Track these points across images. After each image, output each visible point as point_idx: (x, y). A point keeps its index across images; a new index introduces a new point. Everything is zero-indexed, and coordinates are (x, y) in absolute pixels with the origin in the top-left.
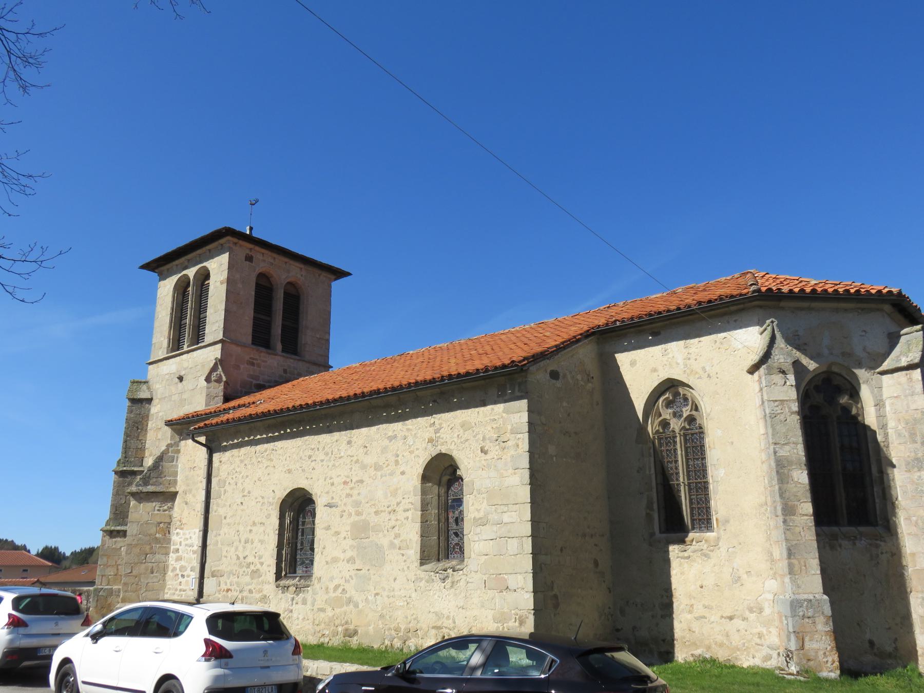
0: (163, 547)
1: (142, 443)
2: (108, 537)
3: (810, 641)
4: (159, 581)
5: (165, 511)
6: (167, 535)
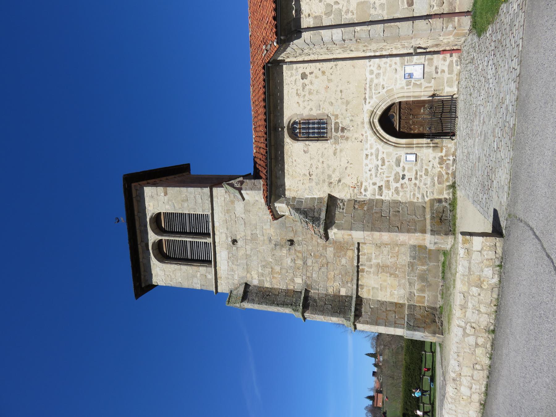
0: (376, 204)
1: (282, 292)
2: (360, 318)
3: (421, 290)
4: (407, 206)
5: (344, 205)
6: (366, 202)
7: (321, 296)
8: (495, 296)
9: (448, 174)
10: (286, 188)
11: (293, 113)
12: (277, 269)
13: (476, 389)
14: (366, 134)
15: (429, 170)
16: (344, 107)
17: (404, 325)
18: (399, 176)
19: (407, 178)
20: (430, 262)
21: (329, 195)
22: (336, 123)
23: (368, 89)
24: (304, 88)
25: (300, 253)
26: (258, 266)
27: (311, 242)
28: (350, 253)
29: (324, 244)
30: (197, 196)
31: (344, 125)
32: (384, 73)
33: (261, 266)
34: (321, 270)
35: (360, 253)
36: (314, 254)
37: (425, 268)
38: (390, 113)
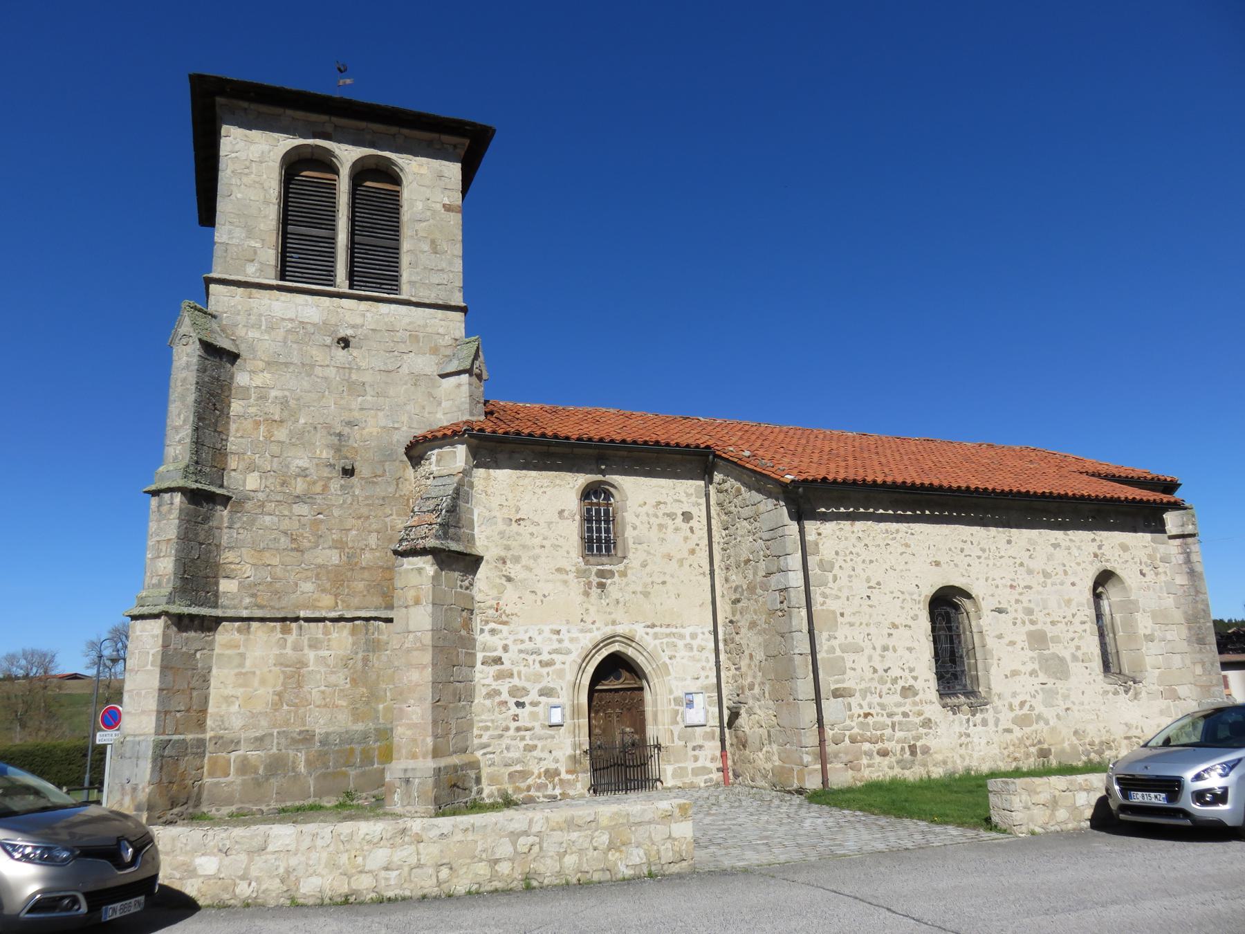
2: (175, 629)
7: (217, 532)
8: (596, 877)
9: (529, 788)
10: (491, 471)
11: (629, 494)
12: (281, 434)
13: (387, 879)
14: (595, 629)
15: (535, 753)
16: (639, 589)
17: (164, 733)
18: (522, 696)
19: (519, 711)
20: (317, 779)
21: (482, 558)
22: (612, 574)
23: (668, 631)
24: (668, 515)
25: (323, 490)
26: (285, 390)
27: (350, 514)
28: (327, 600)
29: (347, 543)
30: (445, 276)
31: (610, 589)
32: (693, 658)
33: (286, 396)
34: (282, 535)
35: (327, 623)
36: (322, 521)
37: (302, 768)
38: (625, 674)
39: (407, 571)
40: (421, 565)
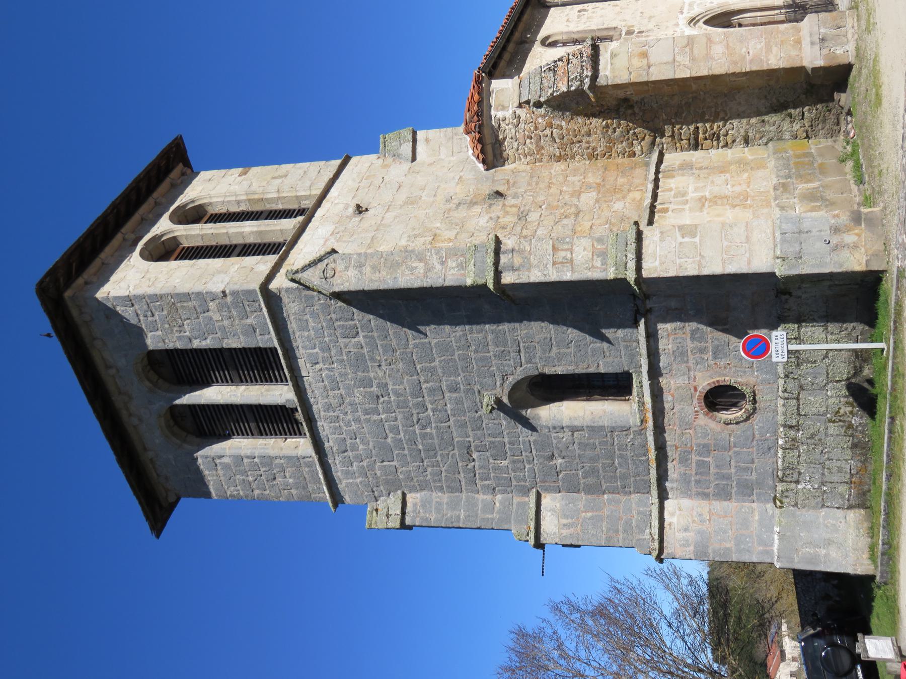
39: (613, 70)
40: (608, 55)
